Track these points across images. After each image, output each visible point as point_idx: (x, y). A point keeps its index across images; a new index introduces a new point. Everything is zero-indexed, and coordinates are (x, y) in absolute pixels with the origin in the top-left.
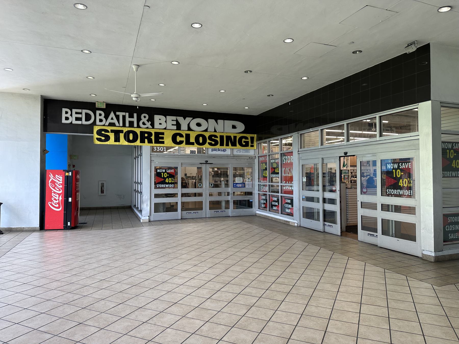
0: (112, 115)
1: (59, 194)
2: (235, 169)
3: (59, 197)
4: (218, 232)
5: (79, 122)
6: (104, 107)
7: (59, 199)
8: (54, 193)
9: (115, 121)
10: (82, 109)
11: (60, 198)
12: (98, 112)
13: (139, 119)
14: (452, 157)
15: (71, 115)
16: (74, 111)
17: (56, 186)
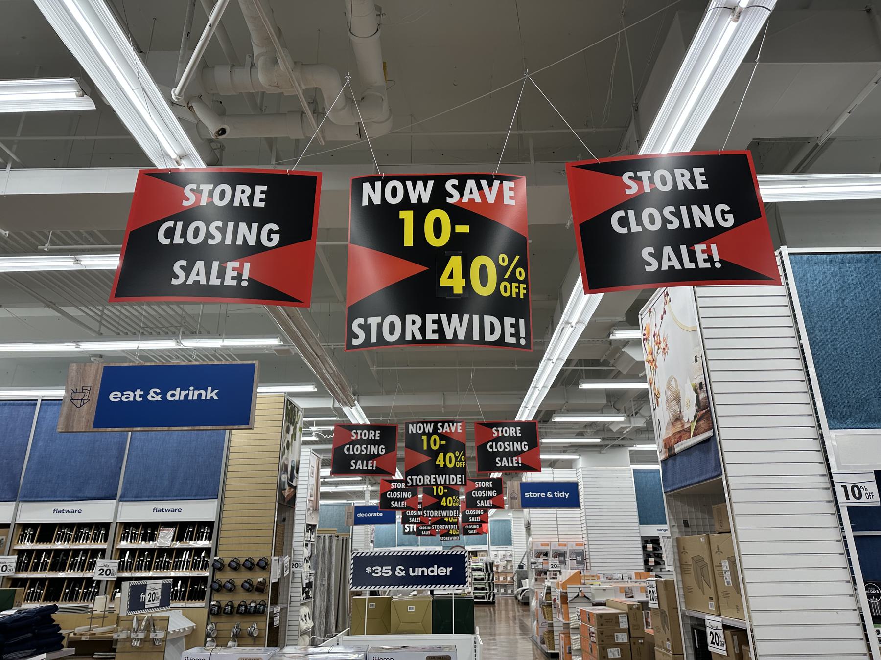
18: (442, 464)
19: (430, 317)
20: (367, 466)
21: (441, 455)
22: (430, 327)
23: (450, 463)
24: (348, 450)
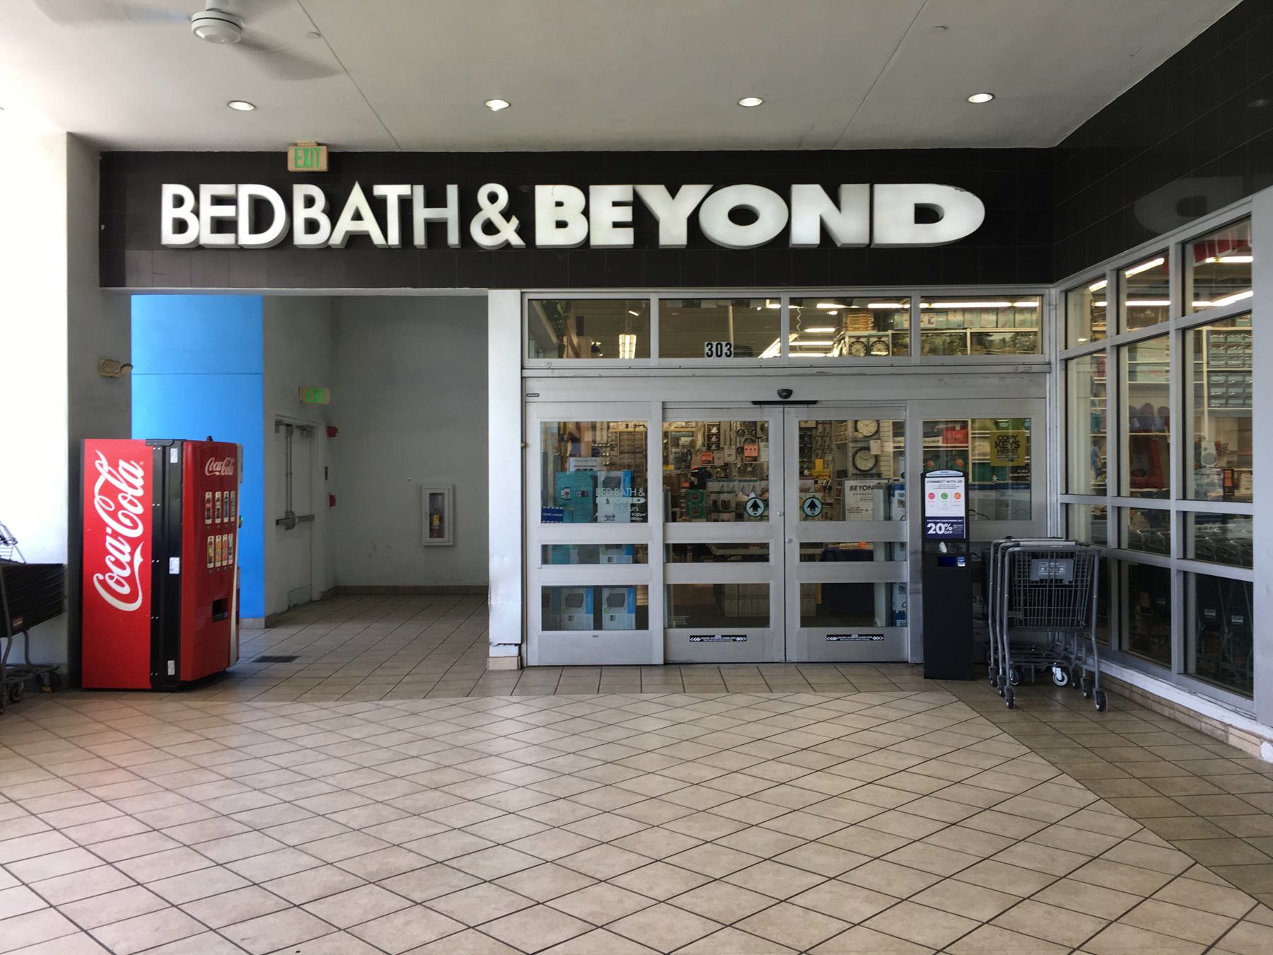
0: (357, 198)
1: (133, 543)
2: (930, 429)
3: (132, 554)
4: (878, 758)
5: (225, 239)
6: (321, 164)
7: (131, 564)
8: (115, 535)
9: (369, 224)
10: (237, 180)
11: (138, 559)
12: (300, 191)
13: (468, 208)
15: (196, 212)
16: (207, 191)
17: (119, 507)
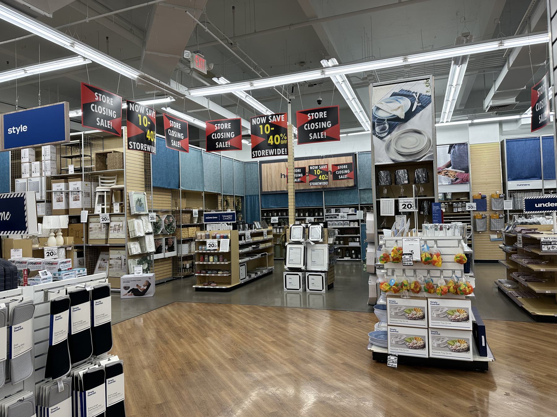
14: (146, 125)
18: (272, 143)
19: (267, 150)
20: (320, 136)
21: (271, 137)
22: (267, 152)
23: (277, 141)
24: (307, 127)
